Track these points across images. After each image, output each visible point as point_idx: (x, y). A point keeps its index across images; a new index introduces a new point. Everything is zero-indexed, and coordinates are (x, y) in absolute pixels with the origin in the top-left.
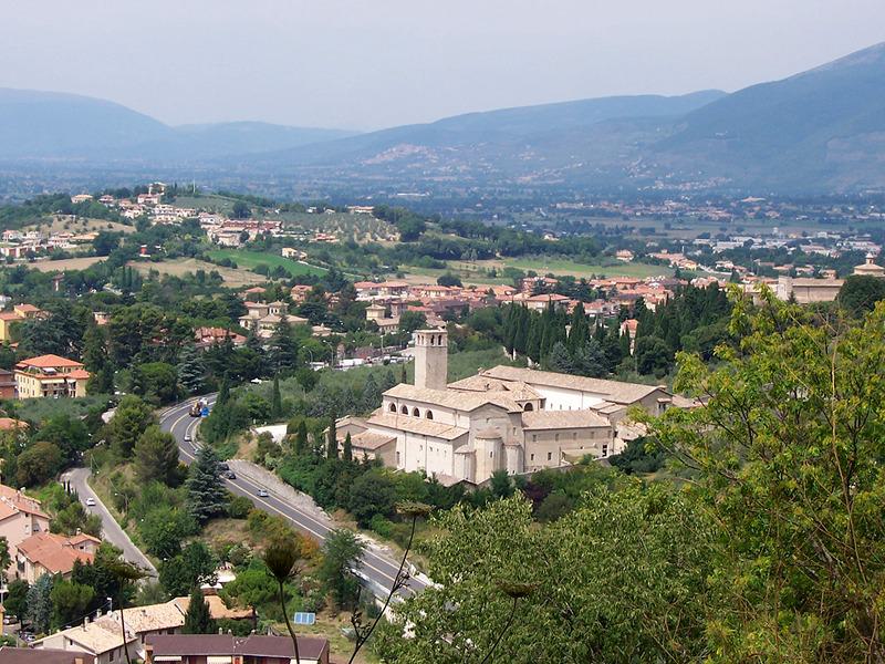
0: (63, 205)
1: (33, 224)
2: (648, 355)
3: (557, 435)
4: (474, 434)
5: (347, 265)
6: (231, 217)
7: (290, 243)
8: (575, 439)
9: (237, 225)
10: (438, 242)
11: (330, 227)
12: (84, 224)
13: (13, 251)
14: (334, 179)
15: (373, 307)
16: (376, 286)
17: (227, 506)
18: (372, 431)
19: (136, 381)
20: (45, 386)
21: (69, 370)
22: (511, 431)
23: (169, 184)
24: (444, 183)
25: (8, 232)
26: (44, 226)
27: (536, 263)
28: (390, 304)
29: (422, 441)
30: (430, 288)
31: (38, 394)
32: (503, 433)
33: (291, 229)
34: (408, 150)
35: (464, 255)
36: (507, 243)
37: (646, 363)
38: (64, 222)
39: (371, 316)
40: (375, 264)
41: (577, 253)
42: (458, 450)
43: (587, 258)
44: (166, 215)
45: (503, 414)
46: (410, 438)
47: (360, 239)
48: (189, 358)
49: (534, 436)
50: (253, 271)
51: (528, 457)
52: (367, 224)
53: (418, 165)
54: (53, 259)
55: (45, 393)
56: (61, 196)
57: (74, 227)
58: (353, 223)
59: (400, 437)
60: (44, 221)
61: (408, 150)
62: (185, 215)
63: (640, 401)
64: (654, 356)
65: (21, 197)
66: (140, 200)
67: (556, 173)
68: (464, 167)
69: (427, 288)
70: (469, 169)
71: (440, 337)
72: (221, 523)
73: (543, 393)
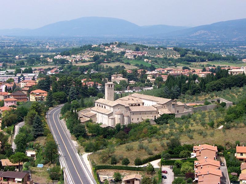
0: (89, 48)
5: (162, 64)
6: (135, 51)
7: (147, 58)
8: (146, 114)
10: (190, 57)
11: (161, 53)
12: (93, 53)
14: (182, 40)
16: (164, 69)
17: (43, 133)
18: (92, 112)
19: (50, 97)
20: (36, 98)
21: (44, 94)
24: (212, 41)
26: (82, 54)
27: (217, 63)
28: (156, 75)
29: (102, 115)
30: (178, 70)
32: (123, 112)
33: (150, 54)
34: (203, 32)
35: (197, 61)
37: (194, 92)
38: (88, 52)
39: (148, 78)
40: (170, 63)
41: (230, 60)
42: (110, 117)
43: (232, 61)
44: (117, 50)
45: (123, 107)
46: (99, 114)
47: (169, 57)
48: (72, 90)
49: (133, 113)
50: (135, 65)
53: (205, 36)
54: (82, 63)
55: (36, 100)
57: (90, 54)
59: (97, 113)
60: (83, 52)
61: (203, 32)
63: (166, 103)
64: (195, 90)
66: (111, 46)
67: (243, 38)
69: (177, 70)
71: (112, 85)
72: (41, 138)
73: (143, 101)
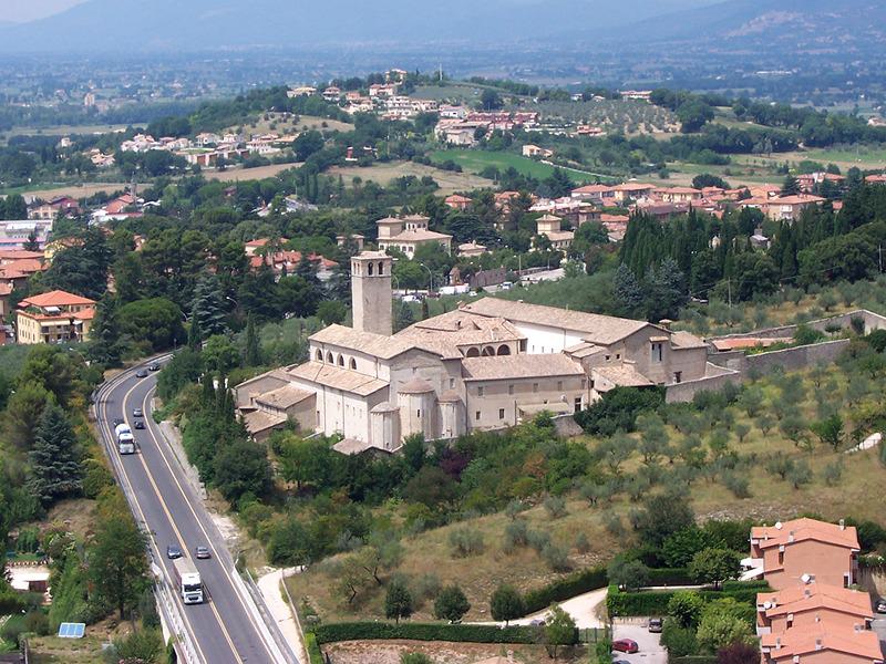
0: (278, 101)
1: (235, 124)
2: (747, 276)
3: (511, 387)
4: (396, 387)
6: (478, 108)
7: (535, 139)
8: (535, 391)
9: (485, 118)
10: (725, 132)
12: (295, 123)
13: (202, 158)
15: (544, 218)
17: (79, 484)
18: (294, 385)
19: (106, 323)
20: (45, 329)
22: (448, 383)
23: (410, 72)
25: (202, 135)
26: (247, 127)
29: (339, 397)
31: (38, 339)
32: (436, 385)
33: (549, 121)
36: (812, 131)
37: (746, 286)
38: (271, 120)
40: (637, 162)
42: (376, 408)
44: (402, 108)
45: (434, 361)
47: (631, 131)
49: (480, 389)
50: (480, 175)
51: (473, 416)
52: (641, 112)
53: (791, 36)
55: (47, 338)
56: (275, 90)
57: (280, 127)
58: (626, 112)
59: (320, 392)
60: (246, 121)
62: (424, 108)
64: (753, 278)
65: (216, 93)
66: (373, 92)
68: (848, 37)
69: (670, 190)
70: (854, 38)
71: (381, 266)
72: (70, 505)
73: (524, 332)
